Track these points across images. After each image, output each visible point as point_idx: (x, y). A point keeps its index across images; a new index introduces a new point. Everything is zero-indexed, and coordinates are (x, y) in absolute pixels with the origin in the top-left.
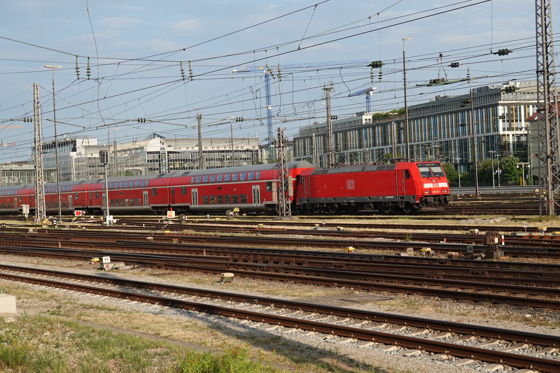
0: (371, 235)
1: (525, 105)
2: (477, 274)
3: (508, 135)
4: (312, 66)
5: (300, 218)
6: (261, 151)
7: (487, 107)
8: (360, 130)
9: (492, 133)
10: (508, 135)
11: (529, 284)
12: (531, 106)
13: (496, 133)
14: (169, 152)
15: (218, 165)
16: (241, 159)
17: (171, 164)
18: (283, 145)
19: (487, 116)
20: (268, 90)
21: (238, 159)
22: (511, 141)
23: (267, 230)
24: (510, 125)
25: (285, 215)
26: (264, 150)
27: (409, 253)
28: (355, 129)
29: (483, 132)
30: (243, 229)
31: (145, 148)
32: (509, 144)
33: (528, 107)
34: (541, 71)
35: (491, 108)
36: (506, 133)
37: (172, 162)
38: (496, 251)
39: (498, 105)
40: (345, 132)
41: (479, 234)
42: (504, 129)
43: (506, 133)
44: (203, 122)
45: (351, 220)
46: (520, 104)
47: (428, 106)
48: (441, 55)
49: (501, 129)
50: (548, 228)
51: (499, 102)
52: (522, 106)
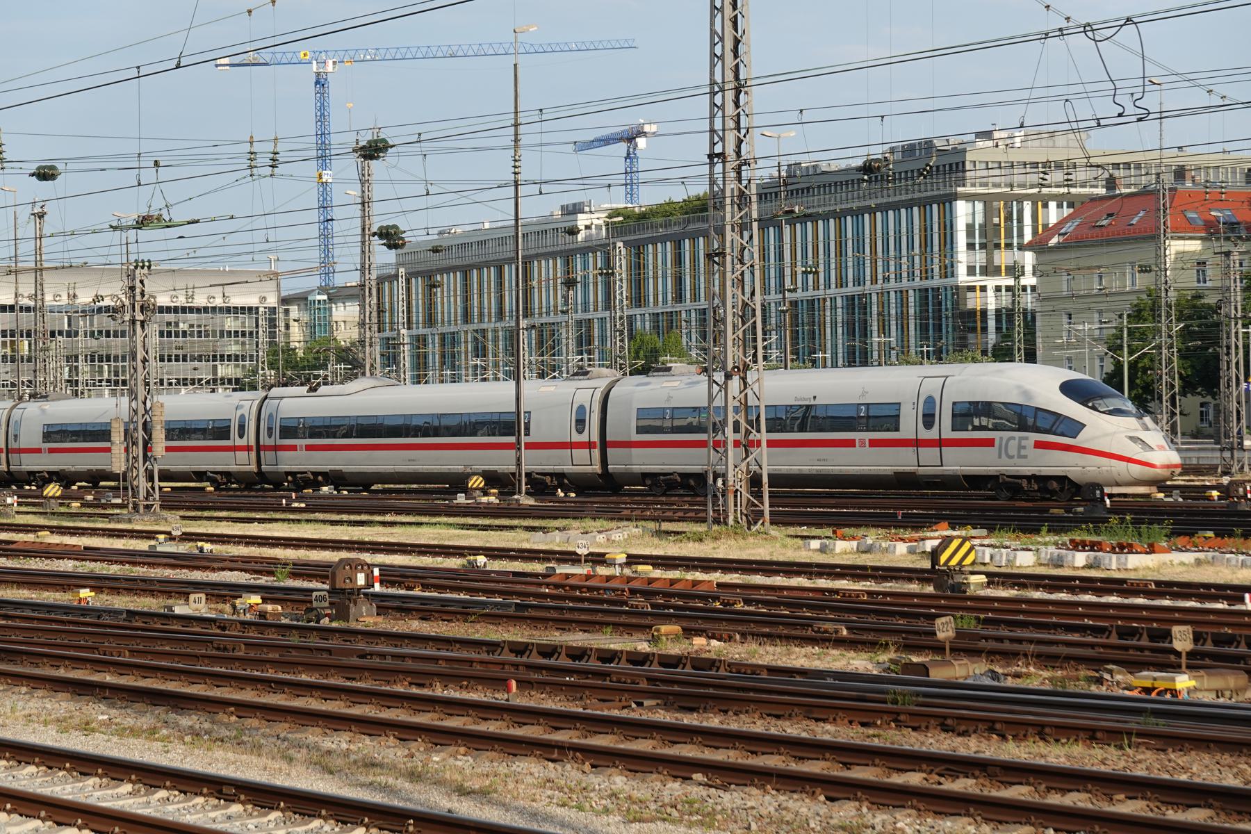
0: (216, 565)
1: (1034, 199)
2: (225, 649)
3: (983, 289)
4: (460, 53)
5: (183, 518)
6: (287, 312)
7: (924, 204)
8: (466, 271)
9: (936, 282)
10: (983, 289)
11: (260, 668)
12: (1052, 205)
13: (948, 281)
16: (222, 335)
18: (142, 318)
19: (678, 260)
20: (323, 123)
22: (992, 307)
23: (58, 548)
24: (990, 259)
25: (141, 509)
26: (294, 311)
27: (193, 605)
28: (553, 255)
29: (911, 276)
32: (984, 313)
33: (1046, 206)
34: (718, 155)
35: (935, 207)
36: (978, 280)
38: (355, 603)
39: (955, 197)
41: (488, 568)
42: (971, 271)
43: (978, 280)
44: (49, 226)
45: (275, 525)
46: (1020, 199)
47: (843, 178)
48: (156, 164)
49: (962, 270)
50: (629, 556)
51: (960, 189)
52: (1027, 207)
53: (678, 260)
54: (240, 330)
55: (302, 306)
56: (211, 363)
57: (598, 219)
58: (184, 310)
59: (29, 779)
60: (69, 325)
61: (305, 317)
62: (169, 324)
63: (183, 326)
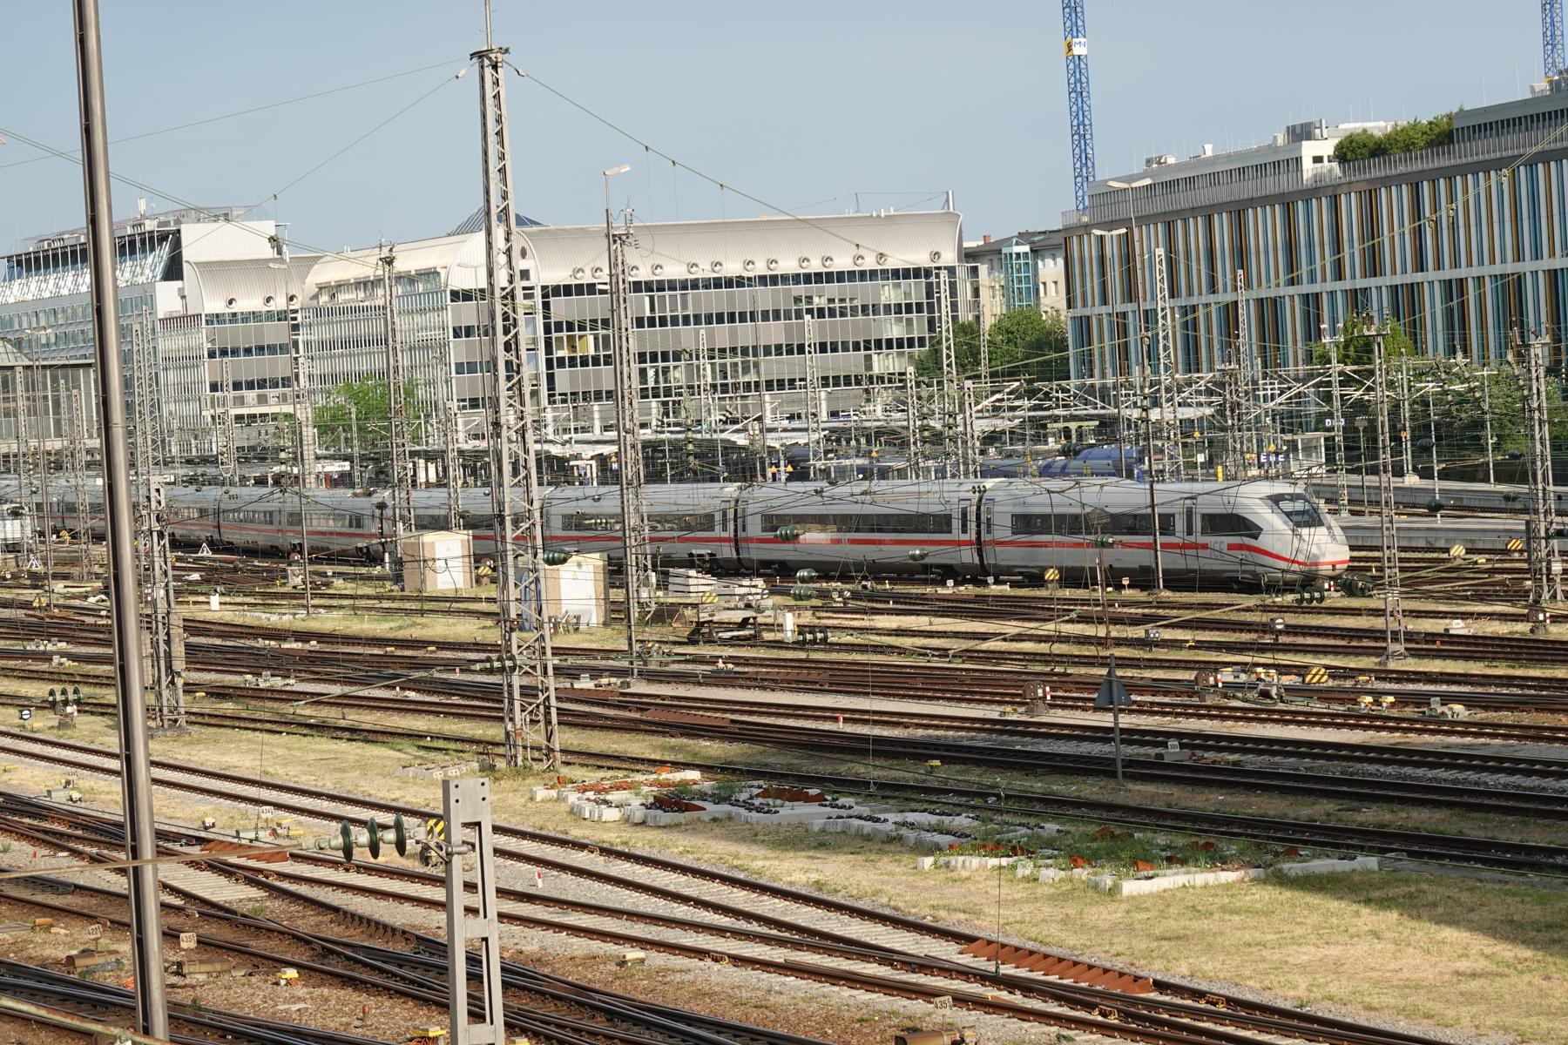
6: (974, 271)
14: (550, 292)
15: (773, 341)
17: (559, 340)
19: (1417, 212)
21: (865, 308)
30: (1142, 664)
31: (443, 273)
37: (564, 334)
40: (1238, 211)
47: (1510, 115)
53: (1417, 212)
54: (903, 302)
55: (996, 262)
56: (863, 352)
57: (1327, 148)
58: (819, 277)
59: (1537, 835)
60: (652, 309)
61: (1000, 277)
62: (797, 300)
63: (818, 302)
